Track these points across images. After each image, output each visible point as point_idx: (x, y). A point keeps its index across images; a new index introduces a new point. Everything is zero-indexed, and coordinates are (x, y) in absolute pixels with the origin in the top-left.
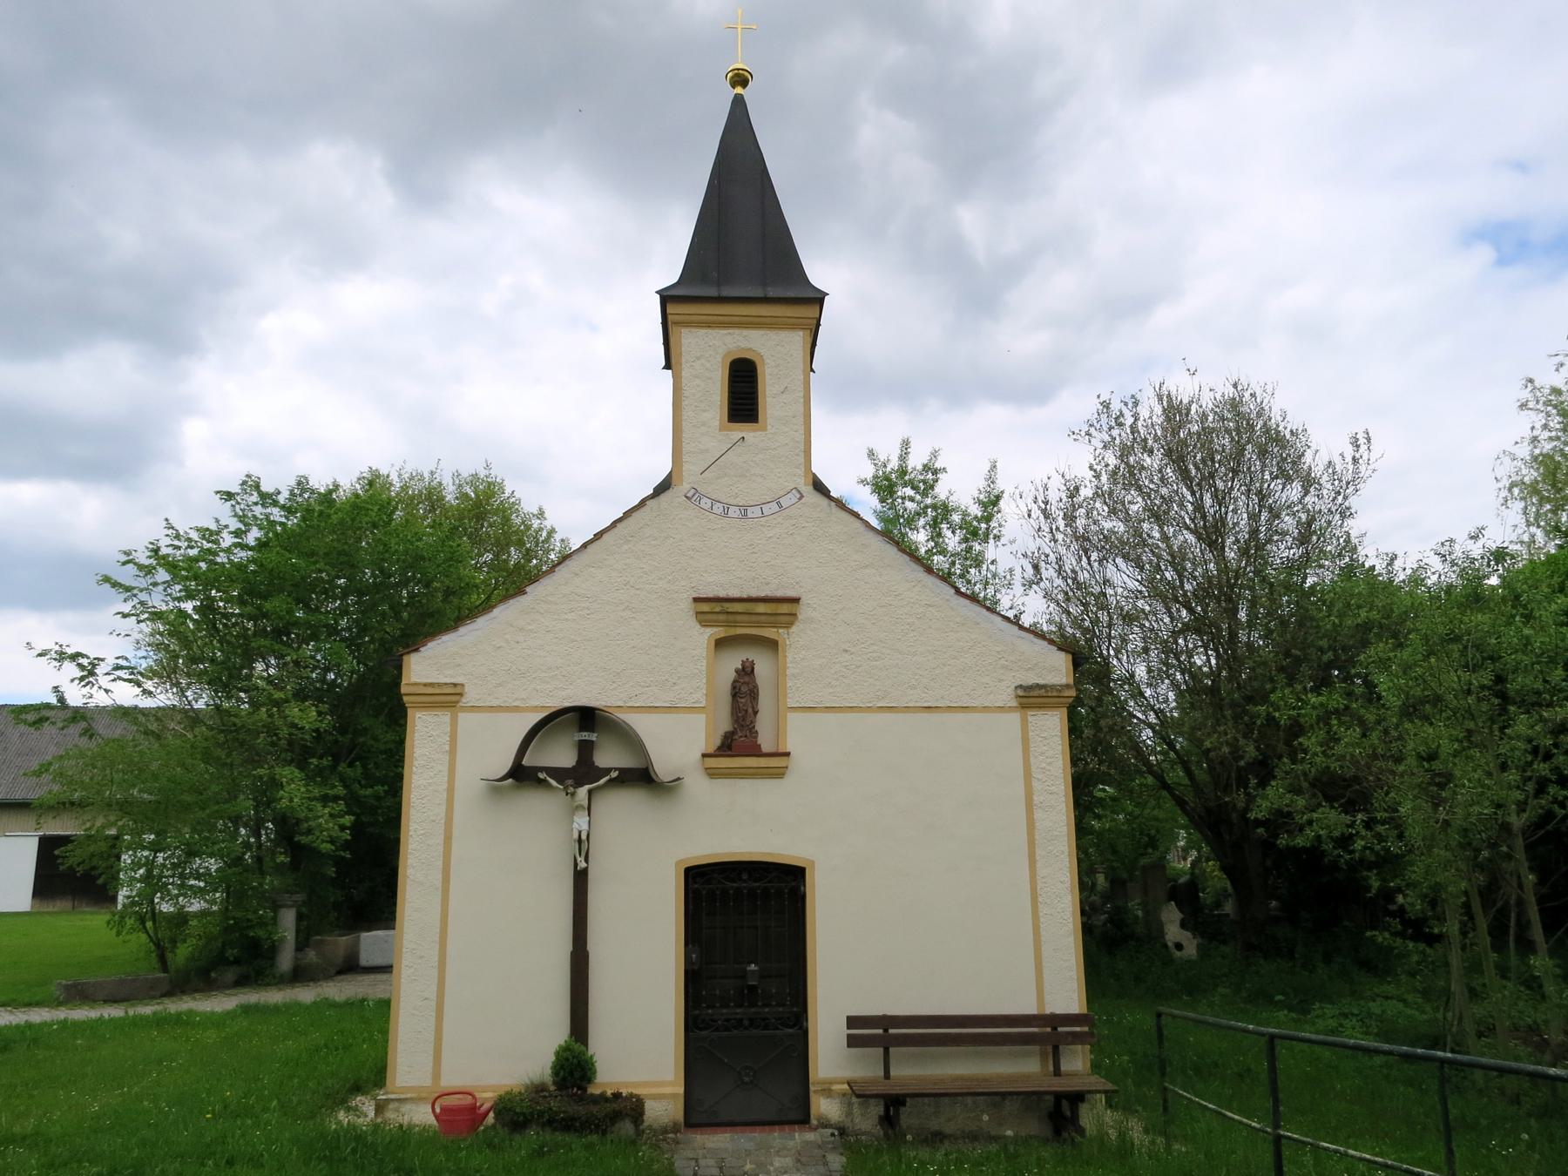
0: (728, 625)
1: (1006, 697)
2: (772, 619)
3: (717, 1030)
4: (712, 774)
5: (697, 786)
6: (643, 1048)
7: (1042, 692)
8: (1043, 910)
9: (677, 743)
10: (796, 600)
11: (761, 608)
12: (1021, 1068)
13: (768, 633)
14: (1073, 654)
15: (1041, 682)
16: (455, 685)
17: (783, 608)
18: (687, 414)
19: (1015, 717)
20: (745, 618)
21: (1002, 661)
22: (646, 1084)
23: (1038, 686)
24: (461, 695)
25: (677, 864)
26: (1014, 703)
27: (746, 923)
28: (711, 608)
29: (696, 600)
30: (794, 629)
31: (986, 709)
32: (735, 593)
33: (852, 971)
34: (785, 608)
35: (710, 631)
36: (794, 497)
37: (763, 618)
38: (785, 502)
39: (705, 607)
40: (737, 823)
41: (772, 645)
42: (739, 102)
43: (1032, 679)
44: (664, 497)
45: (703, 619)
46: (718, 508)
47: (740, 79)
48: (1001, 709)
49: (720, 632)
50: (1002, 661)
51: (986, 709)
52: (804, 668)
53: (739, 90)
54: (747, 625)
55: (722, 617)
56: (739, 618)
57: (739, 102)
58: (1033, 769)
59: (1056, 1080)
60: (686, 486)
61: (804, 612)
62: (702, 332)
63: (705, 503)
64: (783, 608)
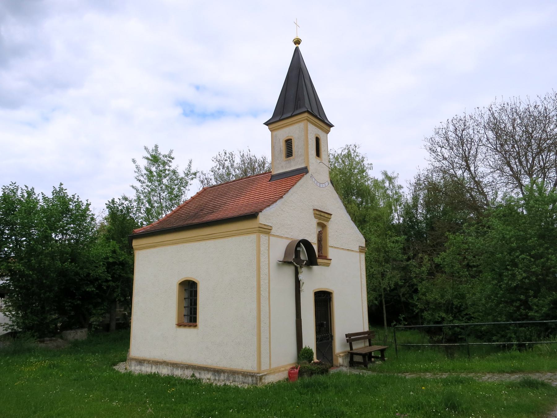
29: (314, 210)
42: (297, 51)
48: (270, 364)
57: (297, 51)
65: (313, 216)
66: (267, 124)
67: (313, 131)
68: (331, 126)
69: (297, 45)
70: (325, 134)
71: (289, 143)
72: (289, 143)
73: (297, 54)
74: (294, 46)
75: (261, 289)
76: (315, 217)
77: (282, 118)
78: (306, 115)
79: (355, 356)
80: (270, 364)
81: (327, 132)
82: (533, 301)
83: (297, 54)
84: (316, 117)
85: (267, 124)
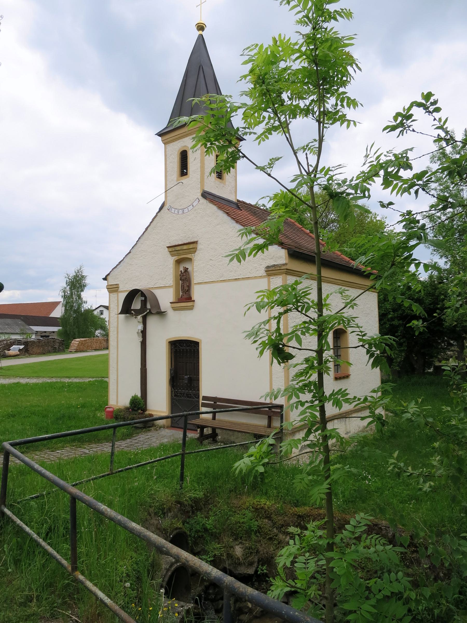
1: (262, 272)
4: (175, 309)
5: (171, 314)
6: (159, 402)
7: (273, 268)
9: (165, 298)
10: (196, 242)
11: (185, 247)
13: (189, 256)
14: (287, 249)
17: (191, 246)
19: (266, 280)
23: (274, 266)
24: (118, 288)
25: (166, 340)
26: (265, 274)
28: (173, 249)
29: (168, 247)
30: (196, 253)
31: (255, 277)
33: (213, 382)
34: (191, 246)
38: (194, 204)
39: (170, 249)
42: (201, 39)
43: (272, 263)
44: (162, 211)
46: (181, 212)
47: (201, 27)
48: (261, 277)
51: (255, 277)
52: (199, 269)
53: (201, 32)
54: (183, 253)
55: (176, 252)
60: (168, 205)
61: (199, 246)
62: (171, 144)
64: (191, 246)
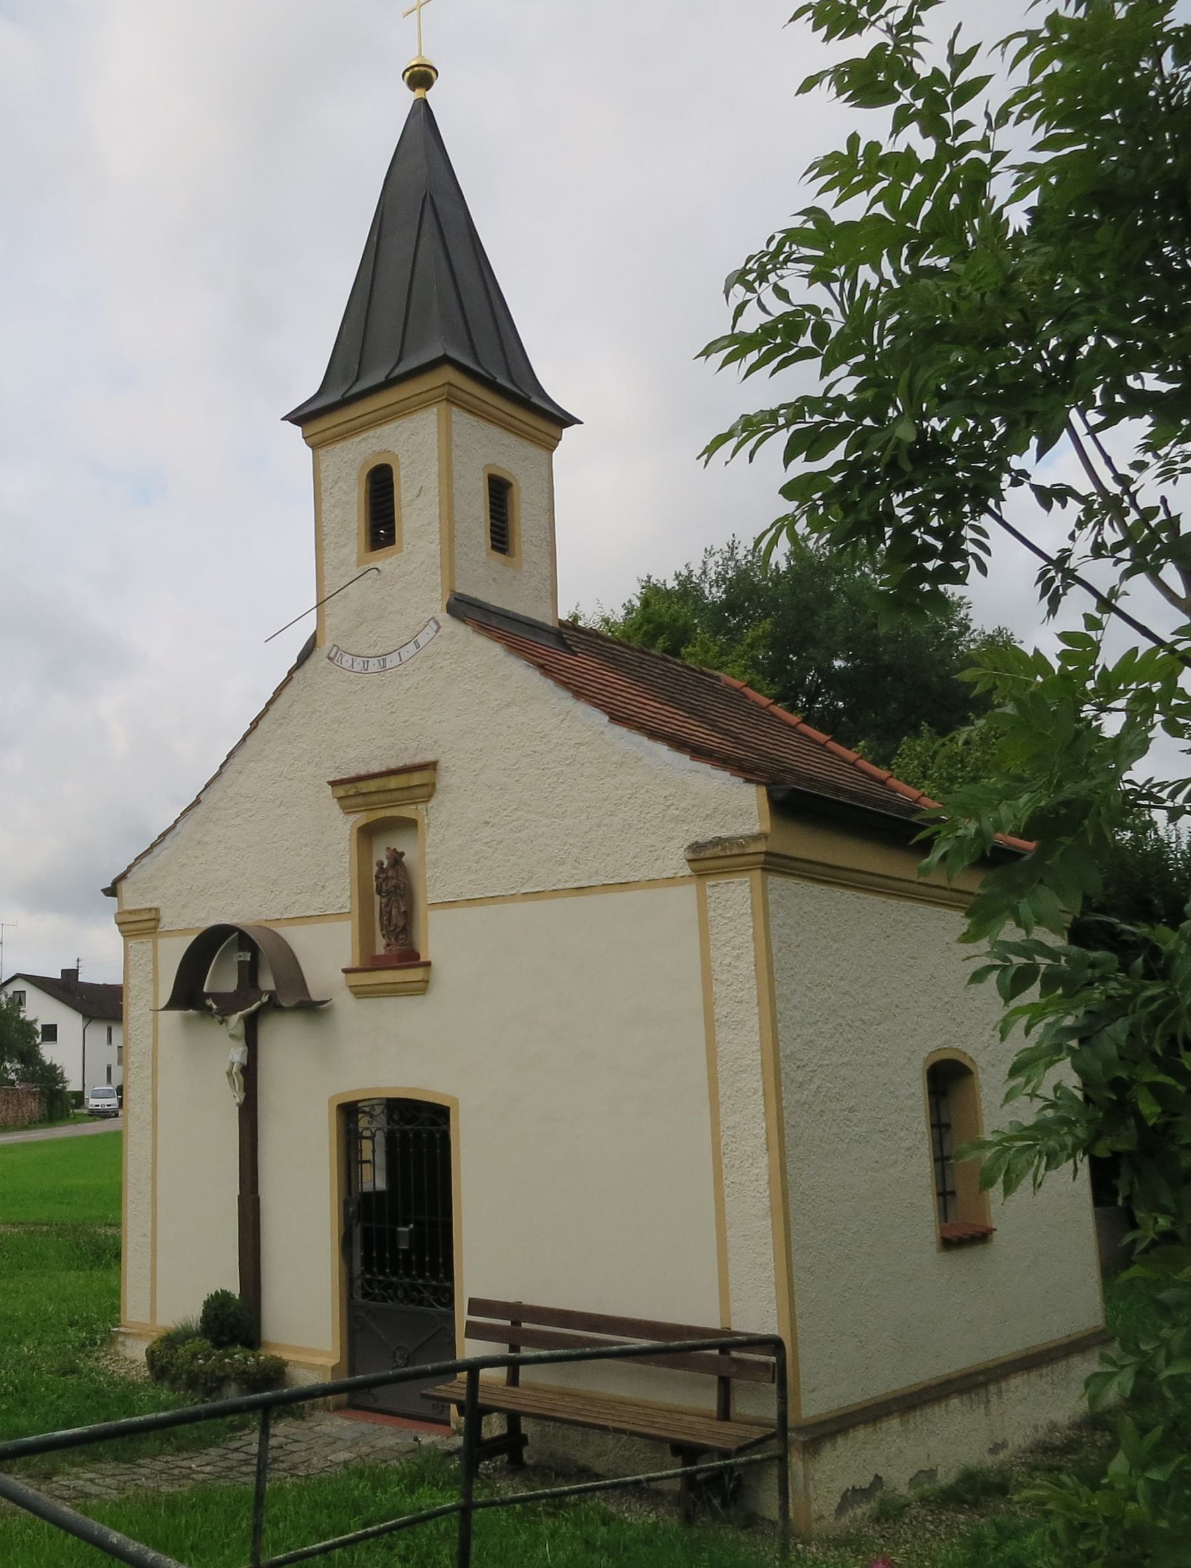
0: (370, 808)
1: (676, 863)
2: (406, 793)
3: (374, 1299)
4: (360, 992)
5: (345, 1004)
7: (718, 851)
8: (729, 1177)
9: (326, 952)
11: (393, 782)
12: (686, 1399)
13: (406, 812)
15: (724, 834)
16: (150, 909)
17: (417, 779)
18: (329, 554)
19: (688, 892)
20: (382, 797)
21: (672, 811)
22: (296, 1350)
24: (157, 920)
25: (330, 1100)
26: (687, 871)
27: (403, 1177)
29: (333, 784)
32: (376, 768)
34: (417, 779)
35: (353, 818)
36: (430, 630)
37: (397, 795)
40: (382, 1050)
41: (410, 824)
42: (423, 117)
43: (709, 831)
44: (309, 665)
45: (347, 804)
46: (374, 665)
48: (671, 880)
49: (362, 818)
50: (672, 811)
52: (443, 855)
54: (386, 805)
55: (359, 800)
56: (375, 798)
57: (423, 117)
58: (715, 965)
59: (726, 1428)
61: (445, 780)
63: (347, 660)
64: (417, 779)
65: (335, 808)
66: (299, 417)
67: (488, 447)
68: (567, 420)
69: (419, 93)
70: (541, 453)
71: (380, 486)
72: (380, 486)
73: (422, 130)
74: (408, 97)
75: (151, 1027)
76: (347, 810)
77: (356, 389)
78: (448, 374)
79: (522, 1368)
80: (671, 880)
81: (551, 444)
82: (1143, 502)
83: (422, 130)
84: (489, 384)
85: (299, 417)
